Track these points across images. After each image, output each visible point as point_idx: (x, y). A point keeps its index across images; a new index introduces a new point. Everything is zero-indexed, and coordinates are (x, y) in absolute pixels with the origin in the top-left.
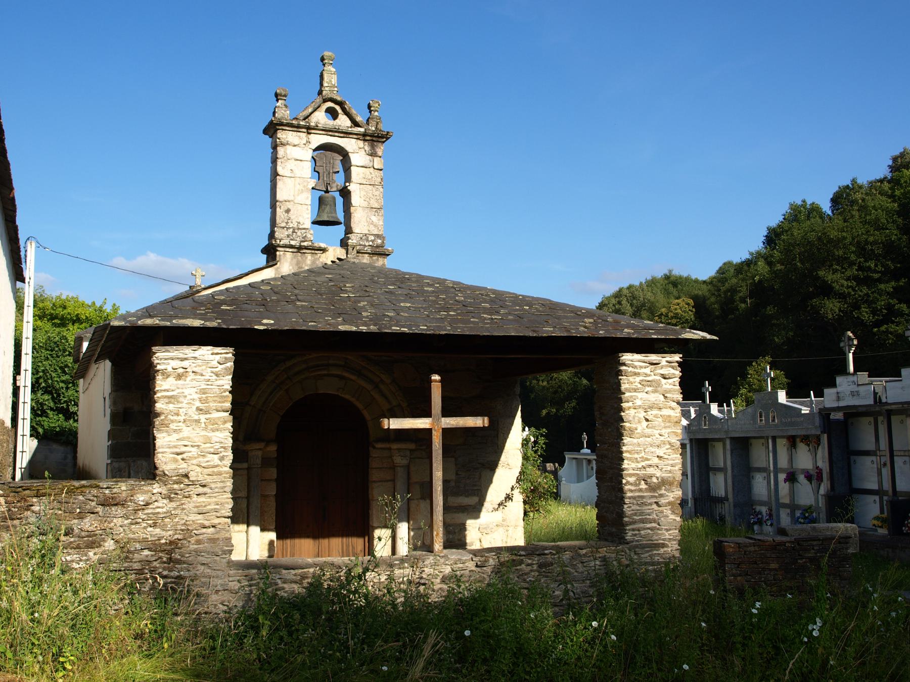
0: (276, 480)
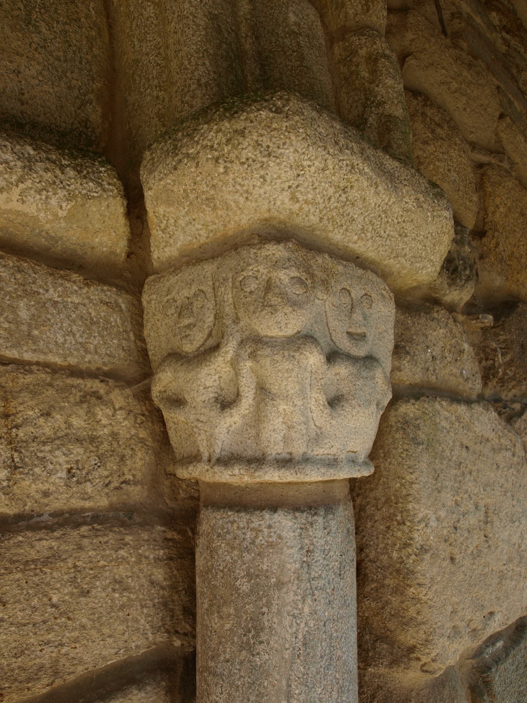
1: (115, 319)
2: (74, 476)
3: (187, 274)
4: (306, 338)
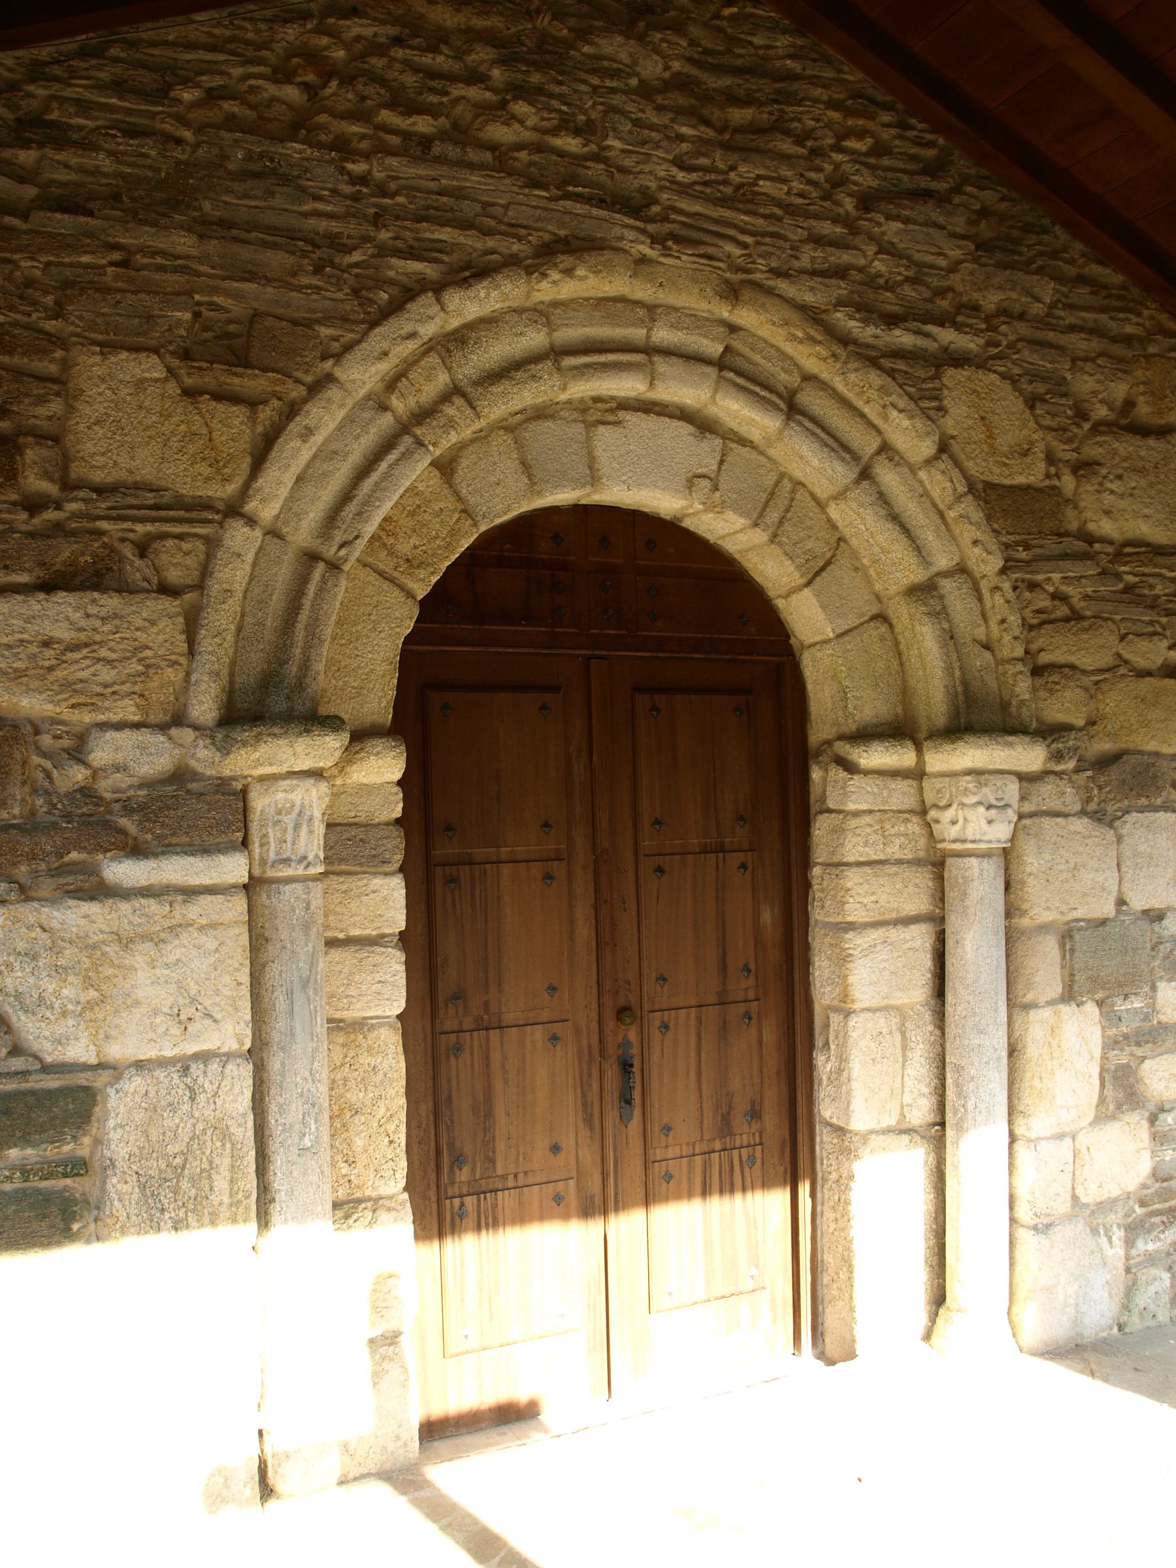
0: (404, 939)
1: (912, 791)
3: (940, 779)
4: (980, 803)
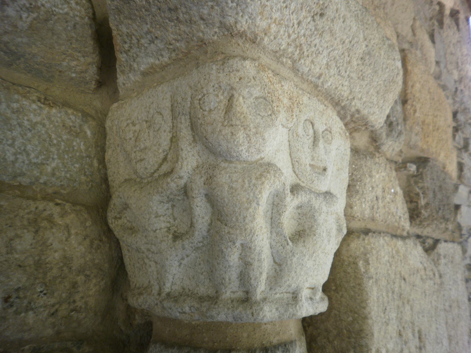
2: (11, 306)
